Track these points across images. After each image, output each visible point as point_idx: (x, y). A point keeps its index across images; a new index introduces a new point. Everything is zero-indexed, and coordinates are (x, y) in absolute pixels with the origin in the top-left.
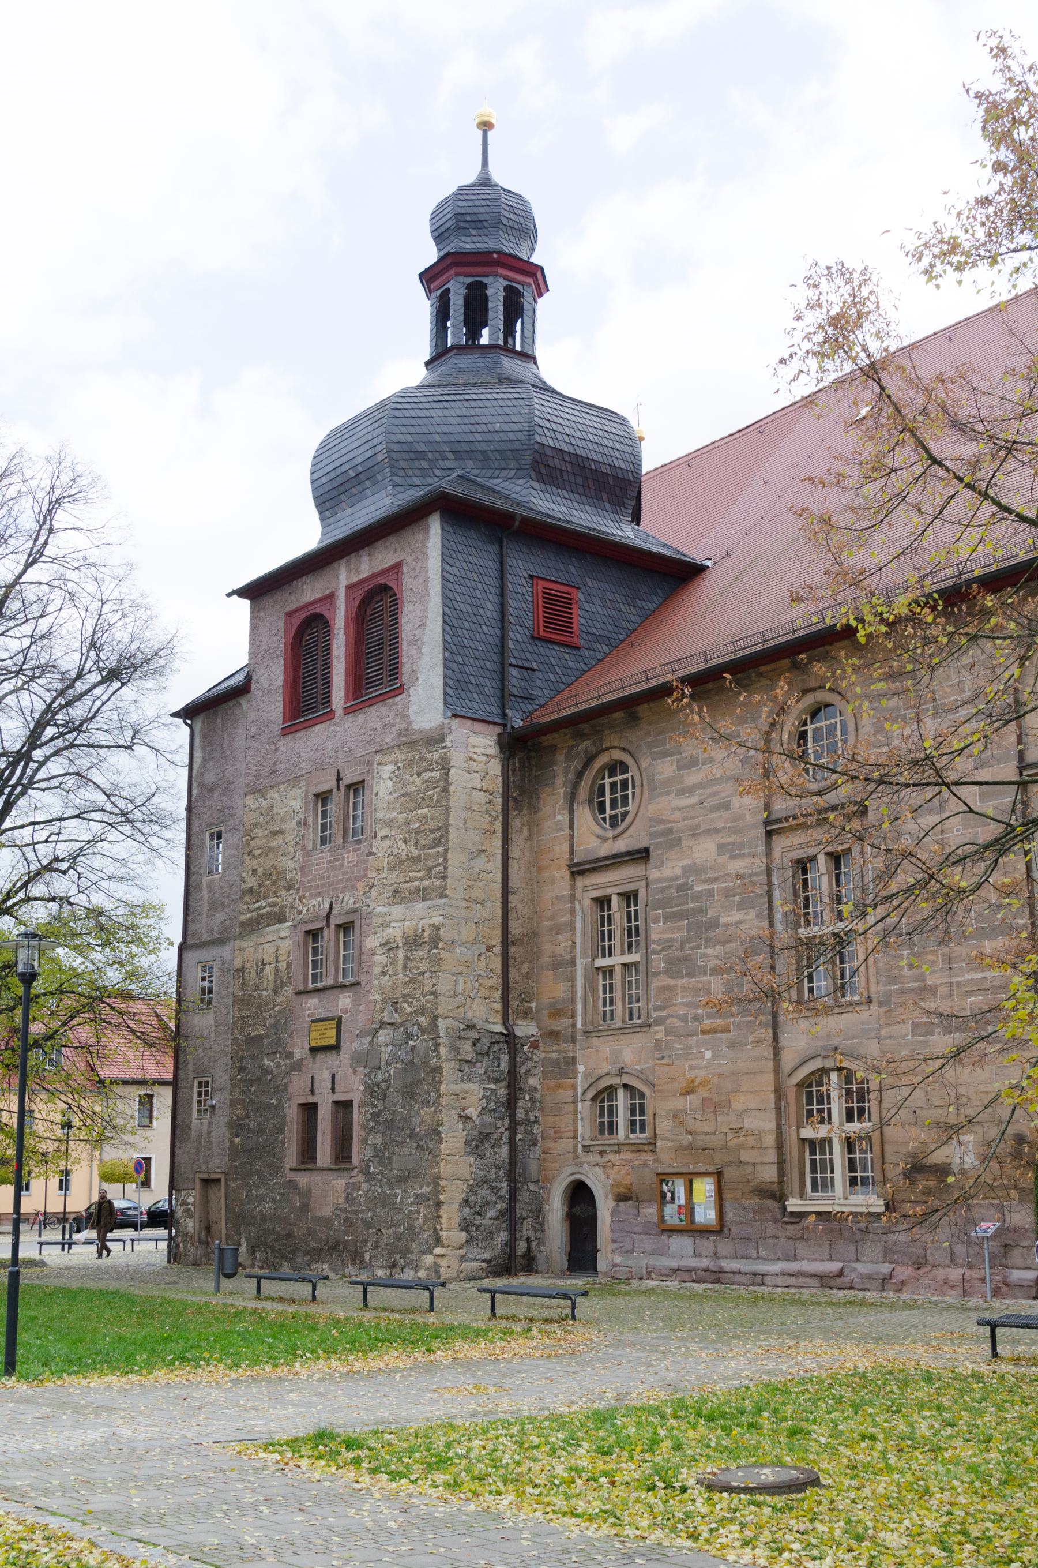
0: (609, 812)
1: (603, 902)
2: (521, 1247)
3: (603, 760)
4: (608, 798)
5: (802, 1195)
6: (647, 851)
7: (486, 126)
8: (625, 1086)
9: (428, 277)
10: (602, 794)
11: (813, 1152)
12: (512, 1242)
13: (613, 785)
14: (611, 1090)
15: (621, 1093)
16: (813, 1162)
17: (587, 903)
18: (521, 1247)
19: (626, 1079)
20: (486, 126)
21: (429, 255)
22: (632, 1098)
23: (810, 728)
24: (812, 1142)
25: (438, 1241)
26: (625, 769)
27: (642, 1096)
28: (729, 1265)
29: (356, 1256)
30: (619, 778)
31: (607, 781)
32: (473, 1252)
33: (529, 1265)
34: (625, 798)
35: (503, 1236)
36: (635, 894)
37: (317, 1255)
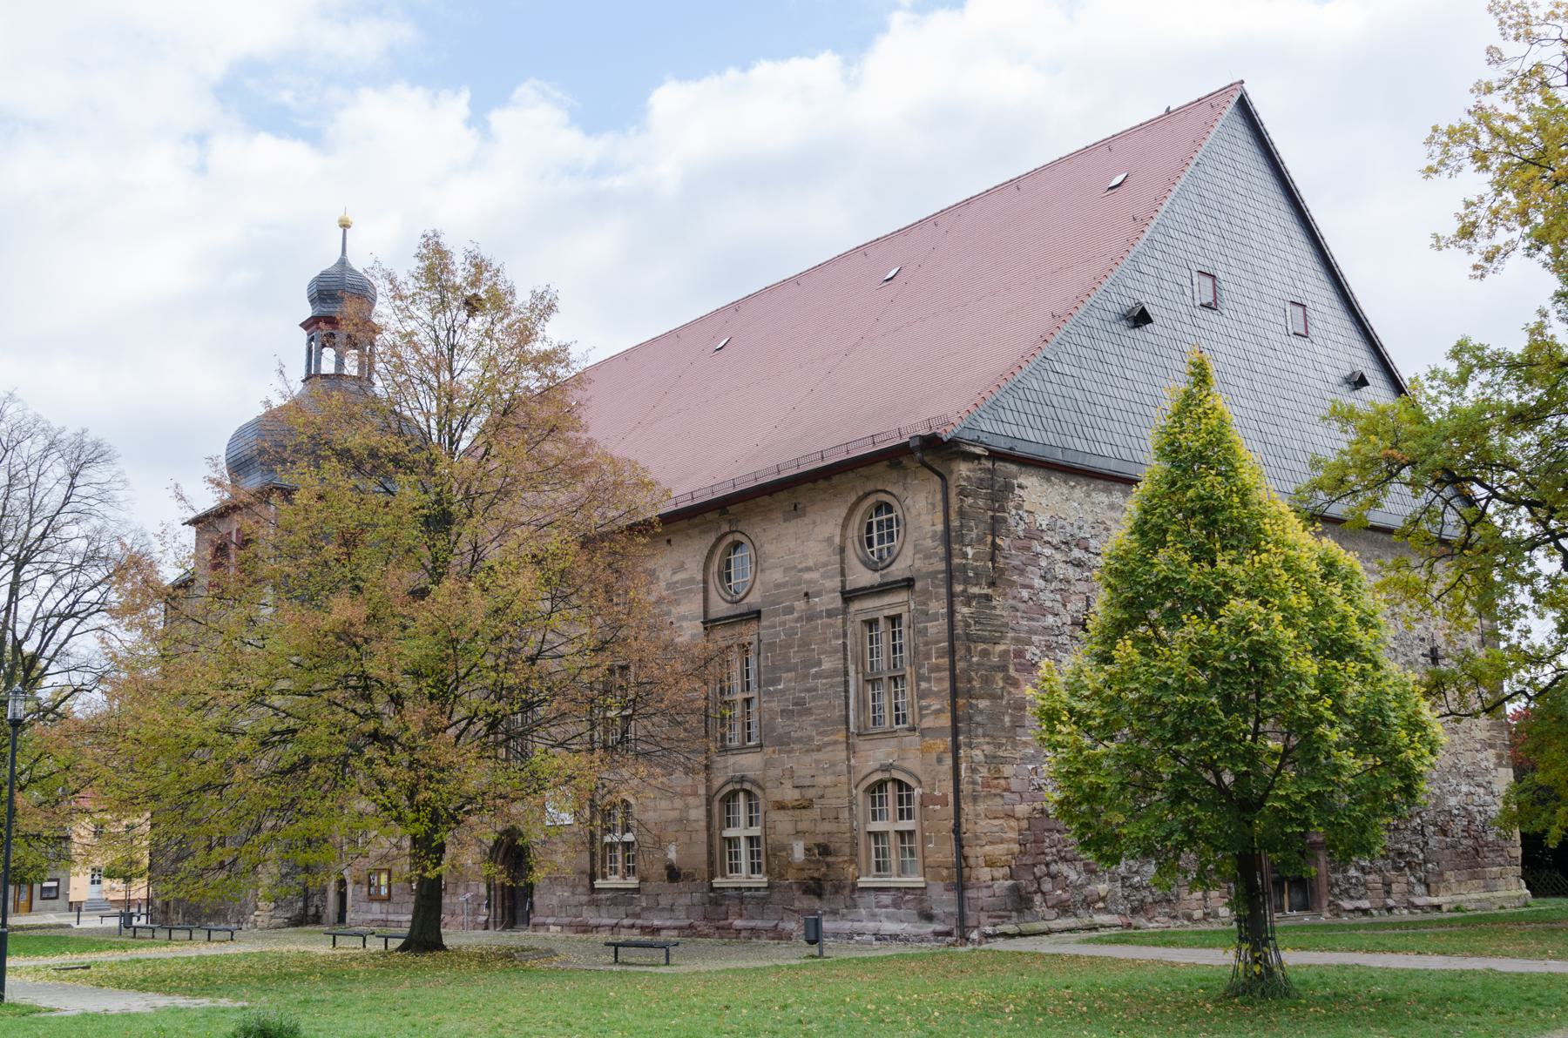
0: (876, 547)
1: (871, 624)
2: (312, 910)
3: (729, 539)
4: (875, 534)
5: (724, 875)
6: (759, 612)
7: (345, 226)
8: (894, 780)
9: (306, 325)
10: (869, 530)
11: (877, 843)
12: (306, 907)
13: (880, 524)
14: (881, 785)
15: (741, 795)
16: (877, 850)
17: (858, 626)
18: (312, 910)
19: (747, 786)
20: (345, 226)
21: (307, 312)
22: (900, 790)
23: (874, 520)
24: (730, 840)
25: (257, 908)
26: (889, 509)
27: (909, 788)
28: (391, 917)
29: (225, 916)
30: (884, 517)
31: (874, 520)
32: (279, 913)
33: (317, 919)
34: (891, 536)
35: (300, 904)
36: (899, 616)
37: (210, 917)
